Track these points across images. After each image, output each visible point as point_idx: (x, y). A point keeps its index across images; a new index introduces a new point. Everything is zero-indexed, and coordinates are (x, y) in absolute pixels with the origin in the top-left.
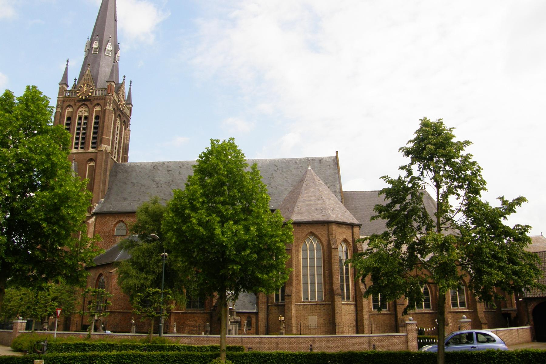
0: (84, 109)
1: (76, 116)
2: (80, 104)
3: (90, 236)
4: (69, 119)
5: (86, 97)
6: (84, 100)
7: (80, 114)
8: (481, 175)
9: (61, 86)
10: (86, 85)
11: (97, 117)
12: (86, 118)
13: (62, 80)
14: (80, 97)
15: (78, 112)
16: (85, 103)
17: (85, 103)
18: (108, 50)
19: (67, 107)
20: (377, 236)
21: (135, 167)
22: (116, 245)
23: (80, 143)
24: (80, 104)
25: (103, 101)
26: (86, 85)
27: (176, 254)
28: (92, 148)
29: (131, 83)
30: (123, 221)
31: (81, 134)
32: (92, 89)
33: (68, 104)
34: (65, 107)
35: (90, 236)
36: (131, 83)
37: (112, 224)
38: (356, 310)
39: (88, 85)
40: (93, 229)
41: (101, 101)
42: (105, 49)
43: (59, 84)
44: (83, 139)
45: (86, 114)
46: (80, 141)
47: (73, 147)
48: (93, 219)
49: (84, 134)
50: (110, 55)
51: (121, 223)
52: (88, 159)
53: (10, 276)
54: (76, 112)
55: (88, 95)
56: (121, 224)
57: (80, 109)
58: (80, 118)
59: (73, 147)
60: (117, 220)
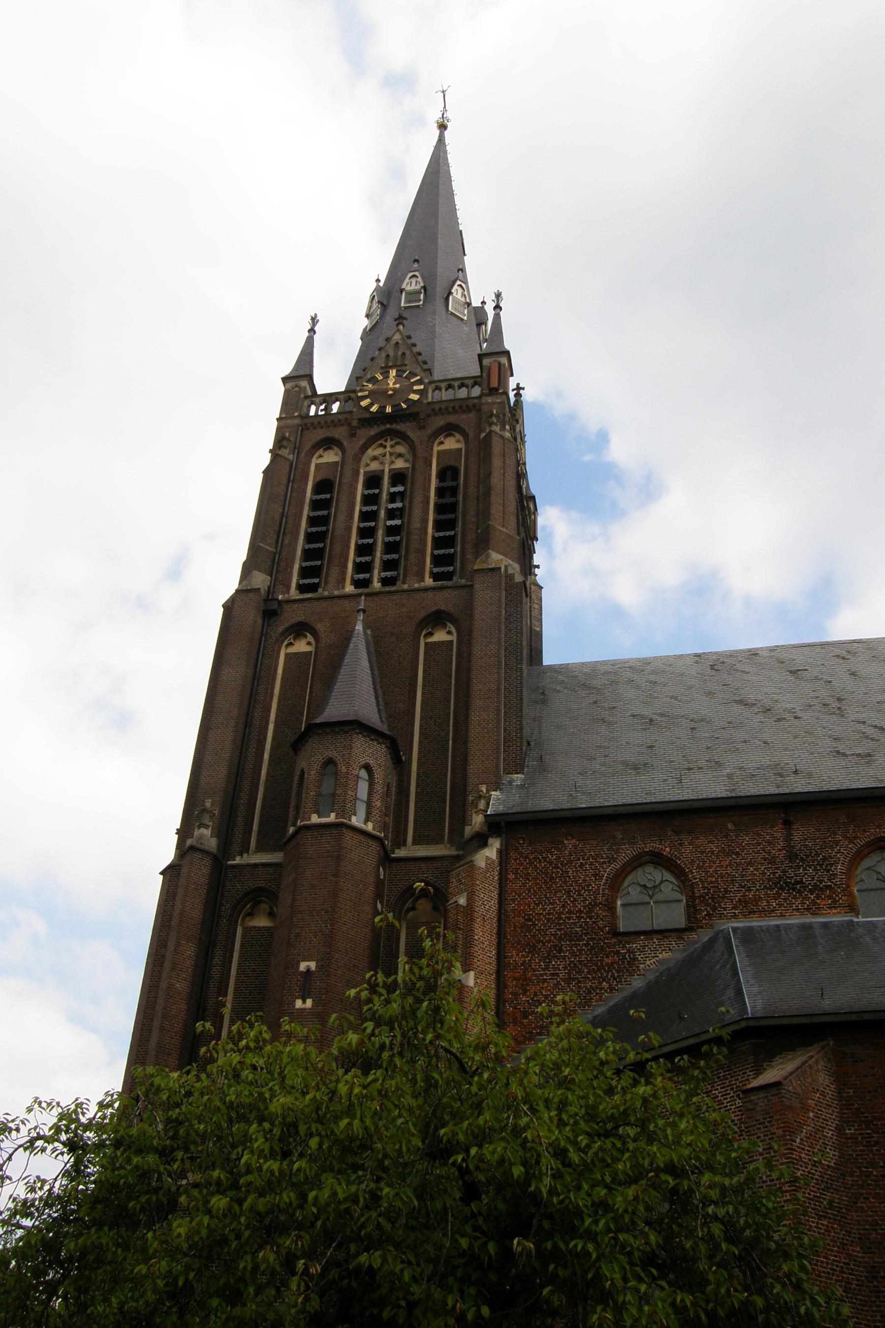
1: (357, 473)
2: (373, 431)
4: (324, 486)
6: (390, 418)
7: (374, 466)
9: (289, 385)
11: (448, 472)
12: (398, 477)
14: (374, 409)
15: (365, 459)
16: (394, 426)
17: (394, 426)
19: (316, 447)
20: (39, 1137)
21: (550, 668)
22: (637, 983)
23: (377, 563)
24: (373, 431)
25: (472, 415)
27: (63, 1133)
30: (658, 860)
31: (380, 533)
32: (420, 382)
33: (320, 437)
34: (308, 446)
37: (597, 876)
40: (493, 904)
41: (464, 416)
42: (447, 299)
43: (285, 380)
44: (390, 548)
45: (400, 464)
46: (378, 554)
47: (348, 580)
48: (491, 852)
49: (391, 531)
50: (465, 318)
51: (649, 869)
52: (423, 614)
53: (71, 1209)
54: (357, 459)
55: (407, 401)
56: (653, 874)
57: (372, 452)
58: (373, 481)
59: (348, 580)
60: (627, 852)
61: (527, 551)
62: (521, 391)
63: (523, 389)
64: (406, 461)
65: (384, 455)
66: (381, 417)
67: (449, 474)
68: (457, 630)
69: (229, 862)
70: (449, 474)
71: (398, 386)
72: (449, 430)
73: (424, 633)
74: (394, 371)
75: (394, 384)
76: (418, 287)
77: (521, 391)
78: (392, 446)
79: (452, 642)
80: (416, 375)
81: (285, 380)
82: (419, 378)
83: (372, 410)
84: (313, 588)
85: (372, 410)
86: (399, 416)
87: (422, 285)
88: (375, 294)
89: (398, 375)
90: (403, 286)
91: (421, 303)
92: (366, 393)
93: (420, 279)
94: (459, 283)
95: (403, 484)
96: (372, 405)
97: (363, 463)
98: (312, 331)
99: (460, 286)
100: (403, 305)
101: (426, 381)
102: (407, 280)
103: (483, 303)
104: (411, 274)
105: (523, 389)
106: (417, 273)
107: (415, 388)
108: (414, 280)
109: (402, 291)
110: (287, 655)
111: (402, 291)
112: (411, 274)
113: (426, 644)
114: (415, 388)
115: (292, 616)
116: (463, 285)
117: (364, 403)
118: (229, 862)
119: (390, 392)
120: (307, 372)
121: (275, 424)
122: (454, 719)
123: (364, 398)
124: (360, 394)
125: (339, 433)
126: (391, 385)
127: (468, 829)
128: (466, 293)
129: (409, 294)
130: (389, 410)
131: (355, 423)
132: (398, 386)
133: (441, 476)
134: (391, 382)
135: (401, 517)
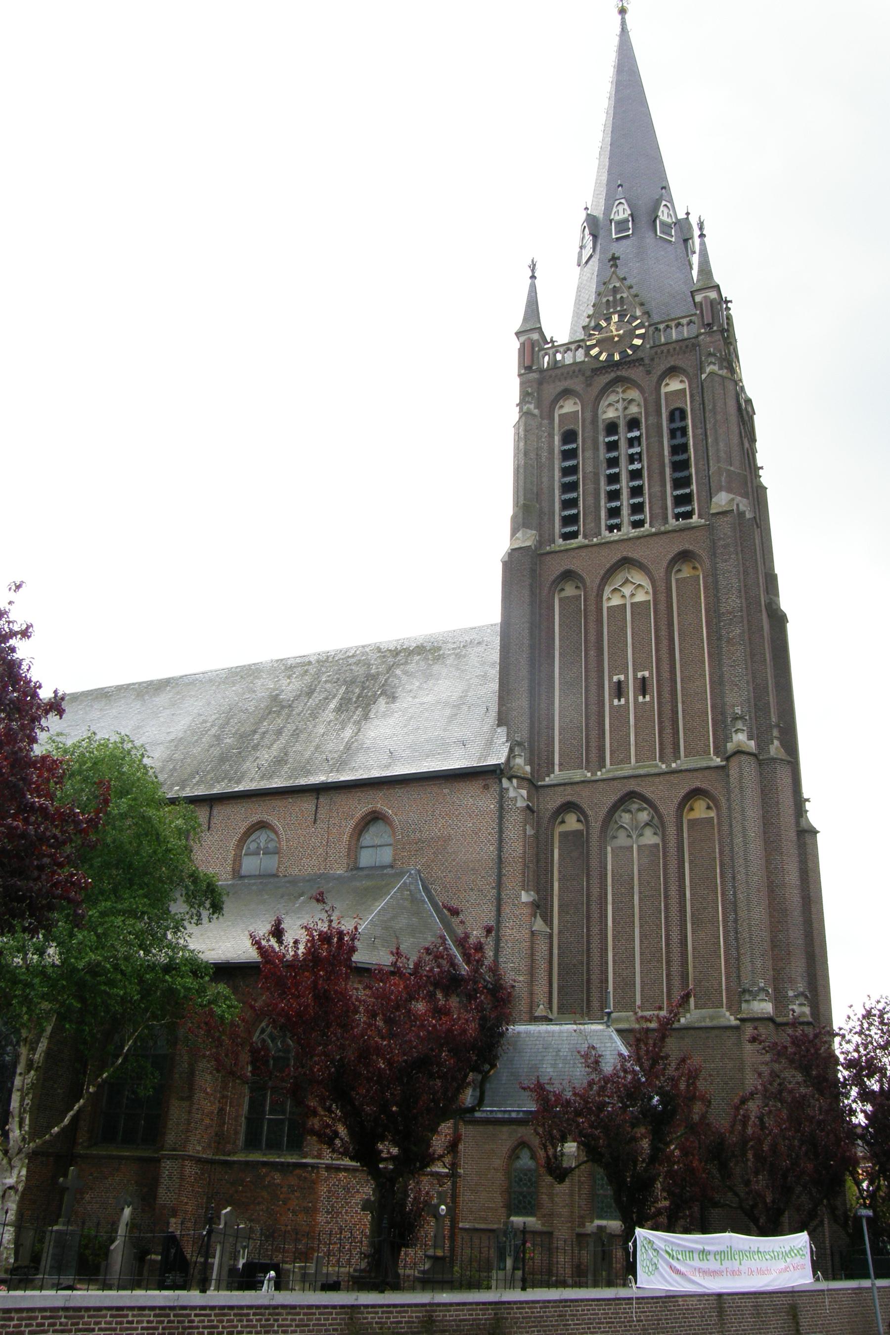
0: (621, 395)
3: (651, 1013)
5: (623, 353)
8: (730, 309)
9: (522, 339)
10: (615, 318)
13: (525, 319)
14: (603, 357)
16: (624, 373)
17: (624, 373)
18: (663, 224)
26: (615, 318)
28: (677, 516)
29: (533, 271)
35: (651, 1013)
36: (533, 271)
38: (255, 876)
39: (622, 316)
42: (655, 221)
43: (518, 334)
50: (673, 239)
55: (632, 347)
61: (746, 418)
62: (729, 305)
63: (731, 301)
64: (647, 593)
65: (618, 402)
66: (610, 365)
67: (677, 413)
68: (686, 377)
69: (540, 783)
70: (677, 413)
71: (621, 332)
72: (672, 371)
73: (674, 570)
74: (616, 316)
75: (617, 330)
76: (626, 215)
77: (729, 305)
78: (624, 392)
79: (685, 389)
80: (637, 319)
81: (518, 334)
82: (639, 321)
83: (601, 359)
84: (574, 535)
85: (601, 359)
86: (626, 362)
87: (629, 212)
88: (585, 224)
89: (621, 320)
90: (612, 217)
91: (631, 232)
92: (594, 342)
93: (626, 207)
94: (664, 203)
95: (639, 429)
96: (600, 353)
97: (605, 598)
98: (533, 277)
99: (665, 205)
100: (614, 236)
101: (647, 324)
102: (615, 210)
103: (688, 214)
104: (618, 202)
105: (731, 301)
106: (623, 201)
107: (638, 332)
108: (621, 208)
109: (611, 221)
110: (559, 415)
111: (611, 221)
112: (618, 202)
113: (677, 580)
114: (638, 332)
115: (557, 567)
116: (668, 204)
117: (594, 352)
118: (540, 783)
119: (616, 339)
120: (538, 326)
121: (517, 381)
122: (714, 734)
123: (593, 346)
124: (588, 343)
125: (577, 384)
126: (615, 333)
127: (729, 745)
128: (671, 212)
129: (618, 223)
130: (617, 357)
131: (588, 373)
132: (621, 332)
133: (672, 418)
134: (613, 328)
135: (640, 460)
